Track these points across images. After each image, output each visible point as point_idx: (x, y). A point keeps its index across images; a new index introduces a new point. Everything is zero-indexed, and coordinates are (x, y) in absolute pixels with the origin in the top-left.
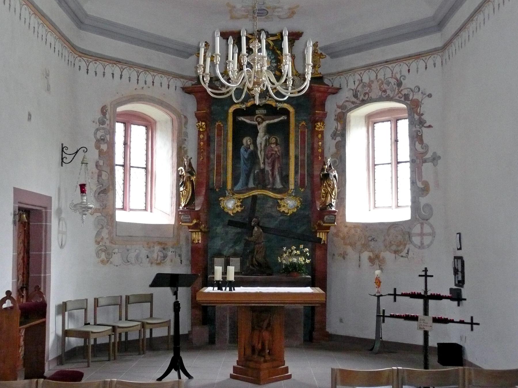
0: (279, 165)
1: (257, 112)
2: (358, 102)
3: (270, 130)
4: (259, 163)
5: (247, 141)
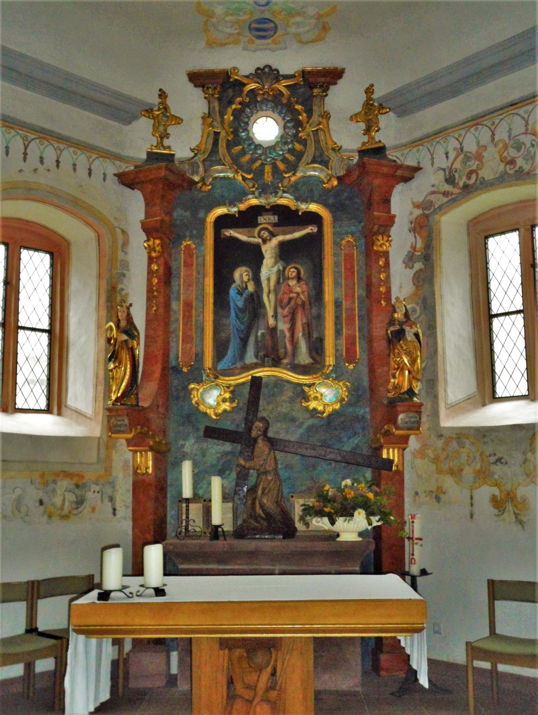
0: (304, 321)
1: (261, 219)
2: (456, 191)
3: (286, 252)
4: (265, 315)
5: (241, 276)
